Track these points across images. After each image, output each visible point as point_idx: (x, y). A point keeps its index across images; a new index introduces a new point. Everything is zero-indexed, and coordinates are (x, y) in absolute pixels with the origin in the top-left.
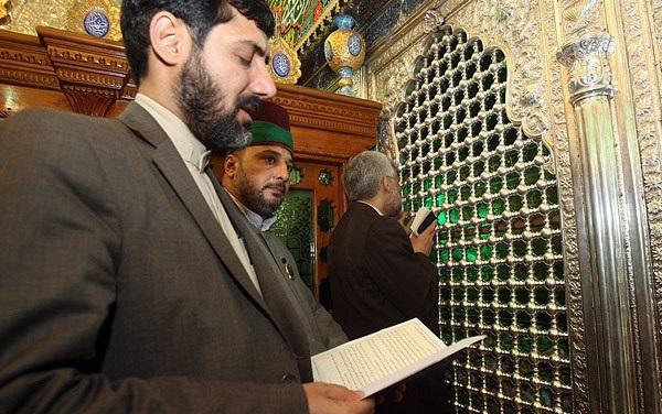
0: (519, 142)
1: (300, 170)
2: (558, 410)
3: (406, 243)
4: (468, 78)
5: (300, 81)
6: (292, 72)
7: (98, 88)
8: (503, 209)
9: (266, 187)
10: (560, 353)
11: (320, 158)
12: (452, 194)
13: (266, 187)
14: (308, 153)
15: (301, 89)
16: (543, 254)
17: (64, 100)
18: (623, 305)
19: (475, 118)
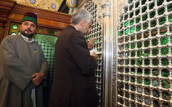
0: (124, 35)
1: (43, 29)
2: (124, 106)
3: (87, 47)
4: (130, 17)
5: (59, 11)
6: (56, 8)
7: (5, 10)
8: (128, 47)
9: (25, 30)
10: (131, 81)
11: (48, 27)
12: (139, 27)
13: (25, 30)
14: (57, 27)
15: (59, 12)
16: (157, 75)
17: (15, 14)
18: (80, 5)
19: (131, 18)
